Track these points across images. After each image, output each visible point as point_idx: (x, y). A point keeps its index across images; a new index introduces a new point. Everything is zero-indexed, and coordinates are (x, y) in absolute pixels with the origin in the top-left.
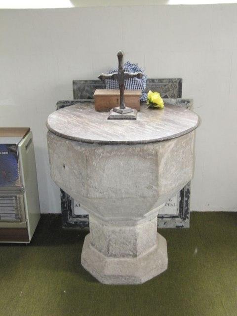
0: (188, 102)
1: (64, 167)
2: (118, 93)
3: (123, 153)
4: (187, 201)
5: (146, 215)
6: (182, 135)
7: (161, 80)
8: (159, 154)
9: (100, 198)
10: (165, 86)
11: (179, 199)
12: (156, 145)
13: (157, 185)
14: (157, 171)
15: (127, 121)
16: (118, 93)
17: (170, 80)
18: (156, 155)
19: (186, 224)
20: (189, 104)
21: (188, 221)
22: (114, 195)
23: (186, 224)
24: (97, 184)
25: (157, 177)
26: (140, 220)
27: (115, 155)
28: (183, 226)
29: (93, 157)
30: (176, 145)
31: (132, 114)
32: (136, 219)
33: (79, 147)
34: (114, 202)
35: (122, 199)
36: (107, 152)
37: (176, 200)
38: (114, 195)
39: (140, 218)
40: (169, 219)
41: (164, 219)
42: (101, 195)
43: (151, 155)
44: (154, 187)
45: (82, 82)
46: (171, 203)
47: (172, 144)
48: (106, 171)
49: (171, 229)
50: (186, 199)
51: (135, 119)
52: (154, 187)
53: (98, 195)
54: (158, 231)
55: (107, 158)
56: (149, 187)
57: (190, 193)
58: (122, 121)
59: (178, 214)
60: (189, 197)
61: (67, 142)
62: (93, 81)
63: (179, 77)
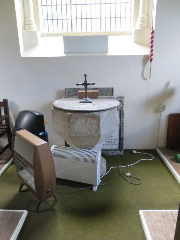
0: (123, 97)
1: (59, 123)
2: (85, 91)
3: (84, 116)
4: (122, 143)
5: (95, 146)
6: (110, 109)
7: (104, 88)
8: (100, 117)
9: (74, 137)
10: (106, 91)
11: (119, 142)
12: (98, 112)
13: (100, 131)
14: (100, 124)
15: (88, 103)
16: (85, 91)
17: (108, 88)
18: (99, 117)
19: (122, 153)
20: (123, 98)
21: (122, 152)
22: (80, 135)
23: (122, 153)
24: (73, 130)
25: (99, 127)
26: (93, 149)
27: (81, 117)
28: (120, 154)
29: (71, 118)
30: (108, 113)
31: (90, 101)
32: (91, 148)
33: (65, 114)
34: (81, 139)
35: (84, 137)
36: (77, 115)
37: (117, 142)
38: (80, 135)
39: (92, 148)
40: (114, 151)
41: (112, 151)
42: (75, 135)
43: (97, 117)
44: (98, 132)
45: (69, 89)
46: (115, 143)
47: (106, 112)
48: (77, 124)
49: (115, 155)
50: (122, 142)
51: (91, 103)
52: (98, 132)
53: (73, 135)
54: (102, 156)
55: (78, 118)
56: (96, 132)
57: (123, 139)
58: (86, 103)
59: (118, 149)
60: (123, 141)
61: (60, 112)
62: (74, 88)
63: (113, 87)
